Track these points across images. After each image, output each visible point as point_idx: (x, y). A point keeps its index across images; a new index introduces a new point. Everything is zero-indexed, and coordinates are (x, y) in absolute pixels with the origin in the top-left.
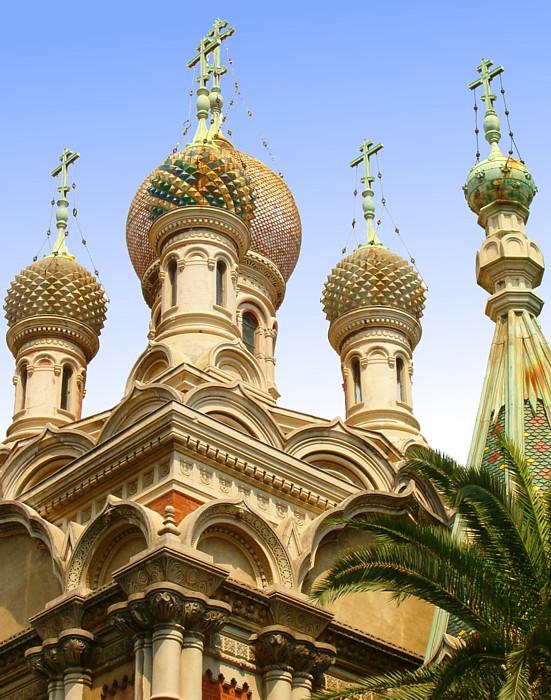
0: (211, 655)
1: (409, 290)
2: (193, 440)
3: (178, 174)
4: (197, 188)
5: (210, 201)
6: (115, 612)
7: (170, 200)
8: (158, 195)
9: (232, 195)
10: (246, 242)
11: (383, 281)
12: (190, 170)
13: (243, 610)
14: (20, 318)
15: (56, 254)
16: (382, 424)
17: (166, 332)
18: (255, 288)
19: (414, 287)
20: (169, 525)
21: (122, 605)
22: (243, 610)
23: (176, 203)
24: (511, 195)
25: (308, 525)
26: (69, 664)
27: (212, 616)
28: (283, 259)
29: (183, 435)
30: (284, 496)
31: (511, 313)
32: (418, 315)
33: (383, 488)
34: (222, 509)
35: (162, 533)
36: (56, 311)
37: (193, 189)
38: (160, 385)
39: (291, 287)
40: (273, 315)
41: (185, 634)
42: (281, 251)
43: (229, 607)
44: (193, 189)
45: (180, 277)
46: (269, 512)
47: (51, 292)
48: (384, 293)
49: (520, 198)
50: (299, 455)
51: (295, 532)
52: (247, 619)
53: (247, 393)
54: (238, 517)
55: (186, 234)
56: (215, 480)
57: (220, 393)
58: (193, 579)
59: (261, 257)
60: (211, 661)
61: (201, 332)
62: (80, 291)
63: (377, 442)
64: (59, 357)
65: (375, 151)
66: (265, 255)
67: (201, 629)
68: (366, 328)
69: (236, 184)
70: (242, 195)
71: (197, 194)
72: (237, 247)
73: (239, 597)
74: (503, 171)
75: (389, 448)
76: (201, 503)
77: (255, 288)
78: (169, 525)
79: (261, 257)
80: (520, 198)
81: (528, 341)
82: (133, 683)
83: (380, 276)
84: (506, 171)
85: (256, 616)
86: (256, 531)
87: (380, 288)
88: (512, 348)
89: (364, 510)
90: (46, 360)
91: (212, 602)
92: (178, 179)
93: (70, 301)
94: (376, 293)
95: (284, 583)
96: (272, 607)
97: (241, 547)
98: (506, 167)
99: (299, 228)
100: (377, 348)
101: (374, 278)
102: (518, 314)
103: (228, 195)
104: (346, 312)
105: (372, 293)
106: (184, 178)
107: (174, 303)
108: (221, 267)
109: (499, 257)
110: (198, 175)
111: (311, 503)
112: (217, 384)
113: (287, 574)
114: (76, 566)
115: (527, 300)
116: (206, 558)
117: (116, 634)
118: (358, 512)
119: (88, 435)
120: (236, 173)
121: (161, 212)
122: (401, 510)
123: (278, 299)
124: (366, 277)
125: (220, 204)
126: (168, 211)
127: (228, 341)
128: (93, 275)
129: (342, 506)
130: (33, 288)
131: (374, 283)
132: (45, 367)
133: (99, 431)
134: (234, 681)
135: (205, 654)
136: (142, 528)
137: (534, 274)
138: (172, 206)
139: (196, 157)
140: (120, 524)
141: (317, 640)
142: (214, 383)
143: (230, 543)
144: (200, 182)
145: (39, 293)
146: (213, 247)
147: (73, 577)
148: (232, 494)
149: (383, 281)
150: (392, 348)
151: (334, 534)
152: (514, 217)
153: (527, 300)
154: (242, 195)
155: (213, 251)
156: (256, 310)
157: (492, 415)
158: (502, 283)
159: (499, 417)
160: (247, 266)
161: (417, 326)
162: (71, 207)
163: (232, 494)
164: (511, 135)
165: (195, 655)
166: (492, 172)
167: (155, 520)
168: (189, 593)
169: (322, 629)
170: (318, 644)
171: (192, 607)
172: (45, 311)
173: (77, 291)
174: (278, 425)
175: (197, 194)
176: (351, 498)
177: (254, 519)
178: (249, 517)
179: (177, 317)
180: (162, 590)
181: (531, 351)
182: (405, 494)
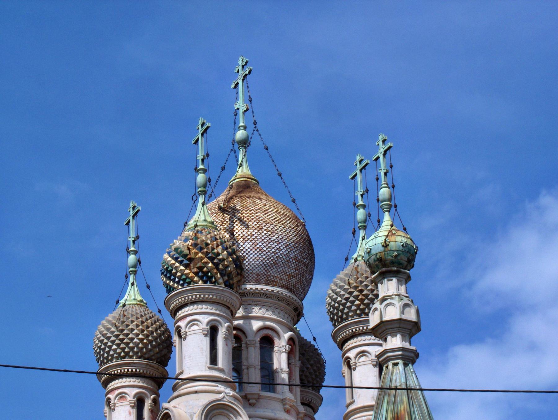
4: (190, 270)
5: (201, 278)
11: (364, 295)
12: (185, 256)
18: (269, 314)
24: (392, 263)
36: (127, 354)
37: (187, 271)
42: (290, 276)
48: (364, 304)
55: (186, 309)
61: (196, 392)
62: (143, 335)
64: (133, 392)
66: (273, 286)
68: (354, 336)
69: (220, 260)
74: (383, 246)
83: (361, 291)
84: (385, 245)
87: (362, 301)
90: (122, 396)
93: (137, 345)
94: (358, 306)
98: (385, 242)
100: (364, 352)
101: (356, 293)
103: (215, 271)
105: (356, 305)
106: (181, 263)
109: (379, 321)
110: (191, 260)
115: (400, 353)
124: (351, 293)
130: (108, 338)
131: (356, 297)
132: (122, 402)
144: (192, 265)
145: (113, 342)
146: (206, 316)
149: (364, 295)
153: (400, 353)
166: (376, 247)
172: (119, 357)
173: (140, 336)
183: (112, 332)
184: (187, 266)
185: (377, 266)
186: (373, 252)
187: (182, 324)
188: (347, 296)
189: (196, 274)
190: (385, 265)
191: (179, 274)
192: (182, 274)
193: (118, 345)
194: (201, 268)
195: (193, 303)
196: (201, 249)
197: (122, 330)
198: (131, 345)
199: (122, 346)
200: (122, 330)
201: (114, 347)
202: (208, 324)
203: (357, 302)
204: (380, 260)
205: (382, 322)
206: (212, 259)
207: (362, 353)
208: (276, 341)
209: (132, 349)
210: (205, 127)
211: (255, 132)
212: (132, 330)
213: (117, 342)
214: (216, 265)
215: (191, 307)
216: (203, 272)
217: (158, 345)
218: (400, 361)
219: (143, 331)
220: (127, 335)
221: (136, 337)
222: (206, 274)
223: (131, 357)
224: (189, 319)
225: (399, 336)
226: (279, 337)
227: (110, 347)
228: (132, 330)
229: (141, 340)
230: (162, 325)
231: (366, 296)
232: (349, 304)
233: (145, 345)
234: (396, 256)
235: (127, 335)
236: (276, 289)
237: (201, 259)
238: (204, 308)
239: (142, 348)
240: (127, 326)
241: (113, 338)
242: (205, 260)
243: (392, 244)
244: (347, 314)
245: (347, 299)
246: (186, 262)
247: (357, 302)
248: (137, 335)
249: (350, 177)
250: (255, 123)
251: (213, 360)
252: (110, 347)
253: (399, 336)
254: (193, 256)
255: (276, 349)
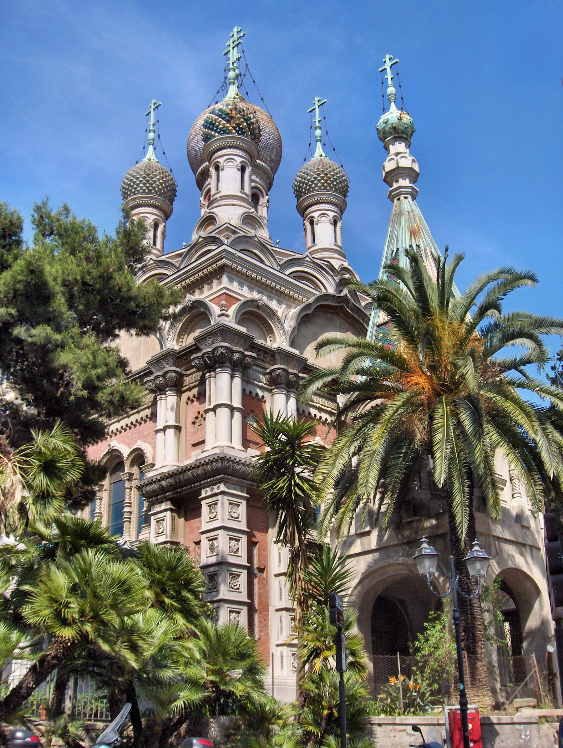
0: (246, 380)
1: (341, 182)
2: (234, 265)
3: (220, 116)
6: (194, 359)
7: (215, 131)
8: (209, 128)
9: (249, 128)
10: (256, 155)
12: (227, 114)
13: (268, 360)
14: (130, 196)
15: (150, 160)
16: (326, 256)
17: (215, 205)
18: (258, 180)
19: (344, 181)
20: (223, 312)
21: (200, 354)
22: (262, 357)
23: (219, 133)
24: (403, 132)
25: (294, 311)
26: (168, 386)
27: (248, 360)
28: (273, 164)
29: (229, 263)
30: (281, 297)
31: (402, 197)
32: (345, 196)
33: (331, 290)
34: (250, 303)
35: (219, 316)
36: (150, 191)
37: (228, 125)
38: (213, 234)
39: (277, 178)
40: (267, 195)
41: (233, 370)
42: (272, 159)
43: (254, 355)
44: (228, 125)
45: (221, 173)
46: (274, 305)
47: (148, 181)
49: (407, 134)
50: (287, 272)
51: (287, 315)
52: (263, 361)
53: (261, 239)
54: (258, 307)
55: (225, 150)
56: (245, 289)
57: (246, 239)
58: (237, 339)
59: (261, 163)
60: (245, 384)
63: (327, 266)
65: (322, 104)
66: (263, 162)
67: (239, 367)
70: (254, 129)
71: (230, 128)
72: (251, 158)
73: (259, 350)
75: (332, 268)
76: (239, 300)
77: (258, 180)
78: (223, 312)
79: (261, 163)
80: (407, 134)
81: (411, 213)
82: (205, 396)
83: (326, 174)
85: (268, 360)
86: (268, 315)
87: (326, 181)
88: (403, 219)
89: (322, 303)
91: (246, 353)
92: (220, 119)
93: (158, 186)
94: (323, 184)
95: (279, 341)
96: (272, 355)
97: (259, 323)
99: (281, 146)
101: (322, 175)
102: (406, 198)
104: (307, 194)
106: (223, 118)
107: (217, 189)
108: (243, 170)
109: (395, 166)
110: (232, 117)
111: (295, 299)
112: (245, 234)
113: (284, 337)
114: (171, 333)
116: (243, 330)
117: (195, 370)
118: (319, 304)
119: (173, 261)
120: (251, 116)
121: (210, 139)
122: (340, 302)
123: (269, 185)
124: (318, 175)
125: (243, 134)
126: (214, 137)
127: (248, 210)
128: (170, 172)
129: (311, 300)
130: (137, 179)
133: (180, 259)
134: (326, 419)
135: (243, 381)
136: (208, 313)
137: (414, 176)
138: (217, 134)
139: (230, 107)
140: (195, 311)
141: (300, 372)
142: (242, 234)
143: (260, 326)
145: (141, 181)
147: (169, 339)
148: (255, 295)
150: (332, 214)
151: (307, 316)
152: (403, 144)
154: (254, 129)
155: (239, 160)
156: (259, 192)
157: (392, 252)
158: (397, 181)
159: (396, 255)
160: (256, 169)
161: (345, 202)
162: (157, 133)
163: (255, 295)
164: (402, 99)
165: (238, 381)
167: (216, 309)
168: (235, 348)
169: (302, 366)
170: (301, 375)
171: (236, 356)
172: (144, 192)
174: (276, 257)
175: (230, 128)
176: (316, 297)
177: (267, 308)
178: (264, 307)
179: (220, 197)
180: (222, 347)
181: (412, 219)
182: (342, 294)
183: (141, 175)
184: (228, 122)
185: (390, 132)
186: (390, 122)
187: (221, 160)
188: (316, 176)
189: (234, 128)
190: (397, 133)
191: (221, 126)
192: (224, 127)
193: (144, 184)
194: (238, 125)
195: (230, 147)
196: (240, 112)
197: (149, 174)
198: (154, 185)
199: (148, 185)
200: (149, 174)
201: (141, 185)
202: (241, 162)
203: (323, 181)
204: (394, 128)
205: (398, 167)
206: (246, 120)
207: (323, 215)
208: (261, 199)
209: (154, 188)
210: (156, 105)
211: (247, 72)
212: (156, 176)
213: (144, 181)
214: (249, 125)
215: (229, 150)
216: (239, 128)
217: (168, 191)
218: (409, 196)
219: (163, 178)
220: (152, 178)
221: (158, 181)
222: (241, 129)
223: (153, 194)
224: (226, 157)
225: (407, 180)
226: (263, 197)
227: (138, 185)
228: (156, 176)
229: (161, 184)
230: (172, 180)
231: (329, 178)
232: (316, 182)
233: (163, 188)
234: (406, 128)
235: (152, 178)
236: (264, 165)
237: (239, 118)
238: (238, 152)
239: (161, 189)
240: (153, 172)
241: (141, 179)
242: (242, 120)
243: (404, 119)
244: (314, 188)
245: (315, 178)
246: (227, 118)
247: (323, 181)
248: (159, 180)
249: (380, 70)
250: (247, 66)
251: (242, 188)
252: (138, 185)
253: (407, 180)
254: (233, 115)
255: (260, 203)
